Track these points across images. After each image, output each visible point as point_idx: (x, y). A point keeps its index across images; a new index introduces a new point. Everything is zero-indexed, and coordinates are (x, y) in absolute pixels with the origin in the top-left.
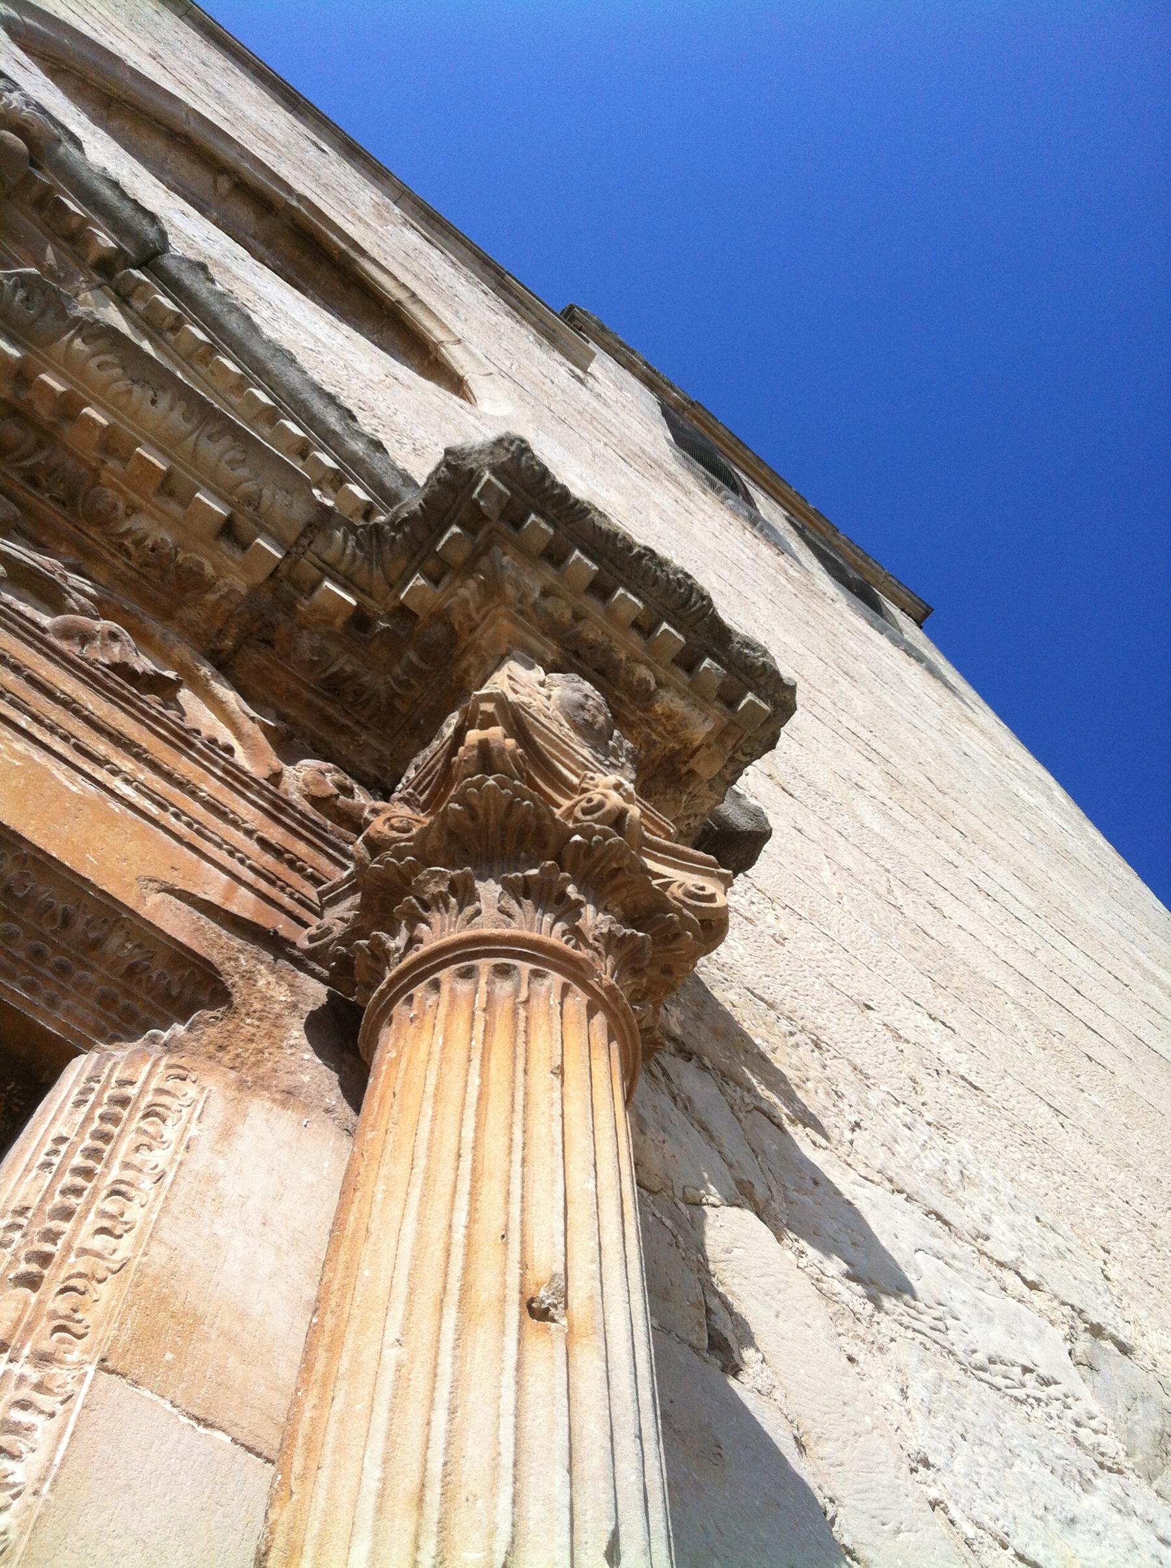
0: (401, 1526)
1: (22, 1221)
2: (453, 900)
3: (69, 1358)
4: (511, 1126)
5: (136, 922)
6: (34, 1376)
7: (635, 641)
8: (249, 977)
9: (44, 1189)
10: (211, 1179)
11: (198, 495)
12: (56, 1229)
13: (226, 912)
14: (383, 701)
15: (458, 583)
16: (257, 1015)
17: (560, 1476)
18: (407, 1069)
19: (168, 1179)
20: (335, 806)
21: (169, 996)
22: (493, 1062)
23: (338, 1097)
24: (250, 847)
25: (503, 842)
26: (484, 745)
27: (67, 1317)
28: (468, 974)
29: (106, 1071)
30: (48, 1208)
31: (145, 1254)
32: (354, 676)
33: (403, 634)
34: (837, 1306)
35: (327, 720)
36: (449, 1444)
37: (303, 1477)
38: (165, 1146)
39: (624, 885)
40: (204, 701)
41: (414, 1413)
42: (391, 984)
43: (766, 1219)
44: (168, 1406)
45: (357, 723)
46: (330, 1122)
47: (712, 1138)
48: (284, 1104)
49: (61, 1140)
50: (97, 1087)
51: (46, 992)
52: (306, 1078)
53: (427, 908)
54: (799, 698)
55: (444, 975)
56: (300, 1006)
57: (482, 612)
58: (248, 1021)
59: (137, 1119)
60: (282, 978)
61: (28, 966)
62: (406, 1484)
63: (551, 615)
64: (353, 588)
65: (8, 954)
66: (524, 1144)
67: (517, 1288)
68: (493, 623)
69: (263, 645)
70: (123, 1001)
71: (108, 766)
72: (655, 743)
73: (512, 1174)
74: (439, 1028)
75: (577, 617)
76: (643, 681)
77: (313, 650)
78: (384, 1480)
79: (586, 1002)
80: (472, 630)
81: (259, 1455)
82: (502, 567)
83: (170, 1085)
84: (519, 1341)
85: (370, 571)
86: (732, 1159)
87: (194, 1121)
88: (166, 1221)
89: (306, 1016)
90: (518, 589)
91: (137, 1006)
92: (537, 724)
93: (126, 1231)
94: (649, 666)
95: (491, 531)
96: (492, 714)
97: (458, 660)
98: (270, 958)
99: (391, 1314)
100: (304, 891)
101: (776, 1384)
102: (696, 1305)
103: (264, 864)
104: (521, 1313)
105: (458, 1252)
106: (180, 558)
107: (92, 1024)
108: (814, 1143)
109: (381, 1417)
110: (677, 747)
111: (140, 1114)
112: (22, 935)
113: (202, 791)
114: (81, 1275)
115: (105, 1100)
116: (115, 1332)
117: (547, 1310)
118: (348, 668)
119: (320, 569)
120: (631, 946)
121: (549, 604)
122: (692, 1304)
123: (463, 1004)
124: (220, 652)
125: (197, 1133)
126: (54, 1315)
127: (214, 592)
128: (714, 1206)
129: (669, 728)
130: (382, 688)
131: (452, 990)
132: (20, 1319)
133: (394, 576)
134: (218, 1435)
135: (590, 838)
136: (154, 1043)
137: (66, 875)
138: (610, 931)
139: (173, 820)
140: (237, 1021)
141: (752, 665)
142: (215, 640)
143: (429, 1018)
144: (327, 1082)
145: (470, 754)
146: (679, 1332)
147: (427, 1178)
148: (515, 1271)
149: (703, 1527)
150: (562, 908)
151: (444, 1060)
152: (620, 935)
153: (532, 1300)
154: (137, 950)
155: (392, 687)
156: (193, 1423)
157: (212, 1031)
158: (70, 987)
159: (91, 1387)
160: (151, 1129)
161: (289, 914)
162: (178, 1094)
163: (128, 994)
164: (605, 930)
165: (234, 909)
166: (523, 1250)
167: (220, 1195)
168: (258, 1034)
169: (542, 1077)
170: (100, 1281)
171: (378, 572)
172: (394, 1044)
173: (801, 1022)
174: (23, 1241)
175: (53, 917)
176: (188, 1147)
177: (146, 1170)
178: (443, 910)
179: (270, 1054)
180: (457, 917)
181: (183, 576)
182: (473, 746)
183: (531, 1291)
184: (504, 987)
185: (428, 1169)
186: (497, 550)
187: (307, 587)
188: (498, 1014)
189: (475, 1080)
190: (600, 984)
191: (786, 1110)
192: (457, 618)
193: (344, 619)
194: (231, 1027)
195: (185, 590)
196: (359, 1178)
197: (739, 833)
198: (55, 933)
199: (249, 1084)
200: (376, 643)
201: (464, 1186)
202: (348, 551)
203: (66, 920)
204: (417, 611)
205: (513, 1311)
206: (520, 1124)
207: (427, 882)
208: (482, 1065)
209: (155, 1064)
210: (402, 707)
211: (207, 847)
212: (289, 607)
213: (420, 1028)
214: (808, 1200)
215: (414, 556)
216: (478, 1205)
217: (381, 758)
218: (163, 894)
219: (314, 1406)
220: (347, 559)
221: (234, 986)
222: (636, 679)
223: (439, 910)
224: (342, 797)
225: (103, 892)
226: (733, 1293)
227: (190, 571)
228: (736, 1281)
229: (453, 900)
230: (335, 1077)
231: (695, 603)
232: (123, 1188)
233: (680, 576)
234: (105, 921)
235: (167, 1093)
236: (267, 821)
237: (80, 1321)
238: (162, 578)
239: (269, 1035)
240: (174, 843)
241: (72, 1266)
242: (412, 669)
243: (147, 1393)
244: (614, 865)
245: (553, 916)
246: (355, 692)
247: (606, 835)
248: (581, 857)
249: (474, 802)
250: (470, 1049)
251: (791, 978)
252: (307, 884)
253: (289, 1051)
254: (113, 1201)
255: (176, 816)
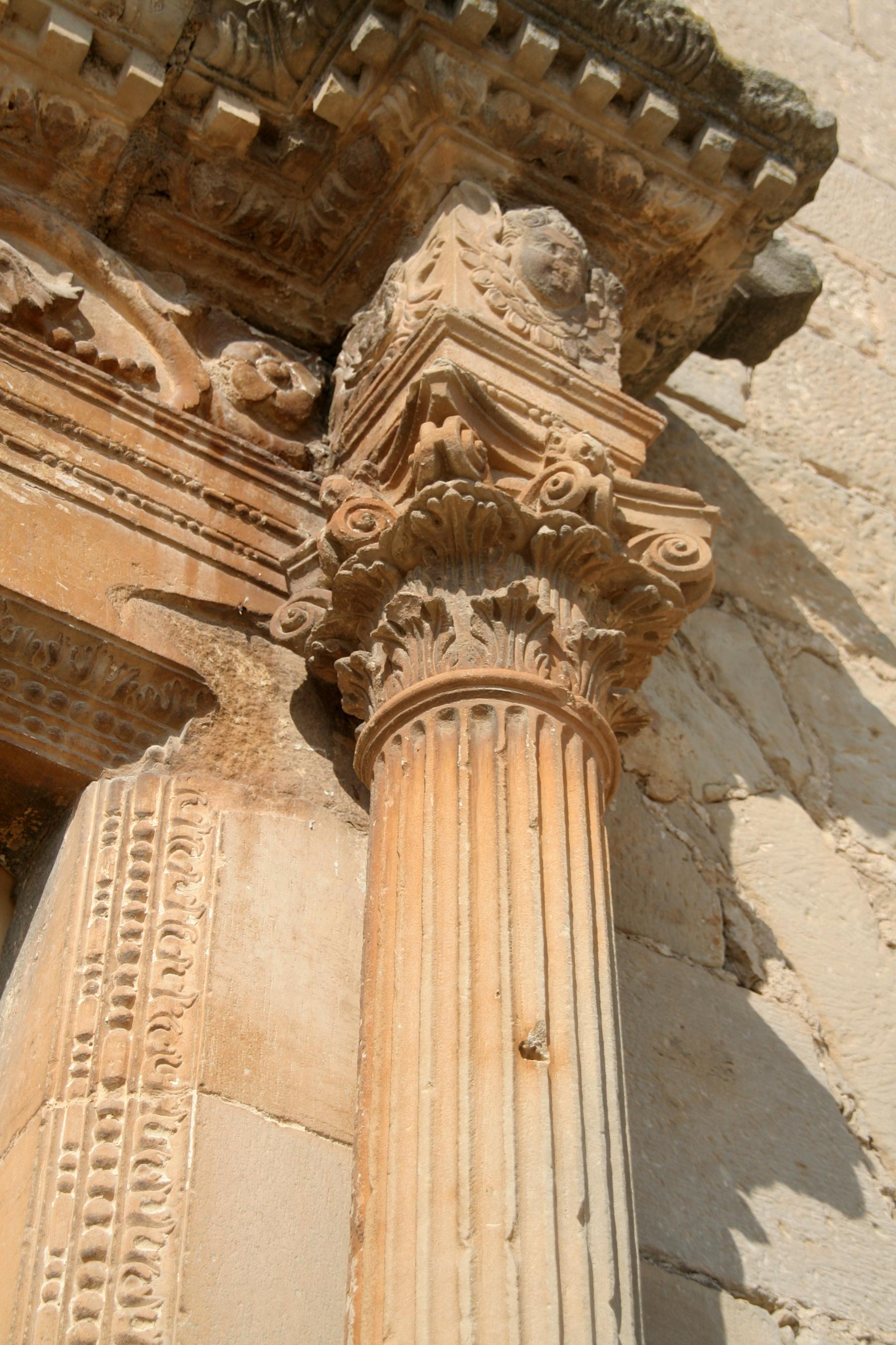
0: (447, 1210)
1: (100, 967)
2: (427, 625)
3: (175, 1084)
4: (498, 890)
5: (117, 645)
6: (154, 1102)
7: (615, 120)
8: (228, 668)
9: (107, 934)
10: (243, 907)
11: (52, 26)
12: (130, 973)
13: (193, 600)
14: (308, 238)
15: (383, 88)
16: (243, 711)
17: (547, 1172)
18: (406, 827)
19: (210, 913)
20: (274, 407)
21: (160, 710)
22: (480, 819)
23: (336, 787)
24: (199, 507)
25: (469, 542)
26: (440, 449)
27: (164, 1052)
28: (448, 716)
29: (123, 802)
30: (117, 952)
31: (209, 990)
32: (270, 212)
33: (321, 148)
34: (881, 888)
35: (244, 275)
36: (472, 1156)
37: (377, 1178)
38: (197, 878)
39: (598, 567)
40: (107, 300)
41: (447, 1133)
42: (379, 722)
43: (804, 798)
44: (255, 1111)
45: (281, 270)
46: (332, 817)
47: (742, 712)
48: (288, 809)
49: (105, 883)
50: (120, 820)
51: (49, 727)
52: (302, 772)
53: (401, 631)
54: (842, 138)
55: (426, 717)
56: (281, 686)
57: (418, 129)
58: (237, 720)
59: (165, 853)
60: (259, 658)
61: (29, 708)
62: (447, 1183)
63: (503, 122)
64: (251, 92)
65: (8, 700)
66: (510, 907)
67: (511, 1038)
68: (433, 143)
69: (156, 199)
70: (119, 722)
71: (45, 458)
72: (647, 256)
73: (502, 939)
74: (429, 785)
75: (536, 111)
76: (628, 180)
77: (217, 193)
78: (432, 1182)
79: (560, 731)
80: (408, 150)
81: (327, 1137)
82: (437, 72)
83: (185, 812)
84: (514, 1079)
85: (270, 67)
86: (764, 734)
87: (217, 851)
88: (218, 956)
89: (289, 697)
90: (459, 98)
91: (132, 725)
92: (497, 337)
93: (187, 968)
94: (632, 154)
95: (418, 23)
96: (444, 400)
97: (394, 189)
98: (241, 637)
99: (422, 1062)
100: (262, 546)
101: (798, 988)
102: (712, 922)
103: (217, 526)
104: (514, 1057)
105: (465, 1011)
106: (43, 105)
107: (96, 750)
108: (880, 676)
109: (425, 1139)
110: (677, 250)
111: (167, 847)
112: (17, 679)
113: (139, 455)
114: (163, 1014)
115: (131, 835)
116: (203, 1061)
117: (534, 1048)
118: (261, 205)
119: (208, 78)
120: (605, 646)
121: (499, 105)
122: (708, 921)
123: (447, 750)
124: (107, 219)
125: (223, 864)
126: (152, 1051)
127: (91, 145)
128: (740, 799)
129: (665, 231)
130: (304, 221)
131: (437, 737)
132: (127, 1057)
133: (301, 70)
134: (295, 1126)
135: (558, 529)
136: (156, 761)
137: (45, 613)
138: (583, 636)
139: (120, 501)
140: (227, 722)
141: (772, 119)
142: (101, 204)
143: (418, 764)
144: (322, 771)
145: (427, 459)
146: (692, 955)
147: (435, 943)
148: (508, 1022)
149: (710, 1139)
150: (532, 624)
151: (438, 820)
152: (592, 638)
153: (523, 1043)
154: (123, 672)
155: (316, 221)
156: (275, 1121)
157: (206, 739)
158: (69, 719)
159: (198, 1107)
160: (181, 863)
161: (253, 580)
162: (196, 821)
163: (122, 714)
164: (577, 637)
165: (200, 594)
166: (514, 1006)
167: (254, 920)
168: (249, 732)
169: (524, 834)
170: (179, 1016)
171: (280, 68)
172: (390, 791)
173: (885, 490)
174: (107, 986)
175: (41, 656)
176: (218, 881)
177: (187, 906)
178: (418, 635)
179: (264, 751)
180: (432, 644)
181: (52, 133)
182: (429, 450)
183: (521, 1038)
184: (484, 727)
185: (435, 934)
186: (427, 49)
187: (196, 102)
188: (480, 762)
189: (466, 846)
190: (573, 708)
191: (845, 641)
192: (387, 137)
193: (248, 142)
194: (222, 731)
195: (56, 150)
196: (380, 934)
197: (776, 299)
198: (45, 670)
199: (254, 795)
200: (288, 165)
201: (465, 953)
202: (240, 47)
203: (54, 657)
204: (335, 122)
205: (509, 1055)
206: (505, 889)
207: (399, 607)
208: (470, 828)
209: (166, 791)
210: (332, 244)
211: (159, 525)
212: (180, 141)
213: (412, 778)
214: (861, 760)
215: (323, 42)
216: (478, 965)
217: (314, 308)
218: (134, 600)
219: (377, 1128)
220: (240, 58)
221: (217, 686)
222: (618, 178)
223: (414, 635)
224: (280, 392)
225: (81, 622)
226: (756, 897)
227: (60, 126)
228: (761, 883)
229: (427, 625)
230: (330, 765)
231: (691, 51)
232: (174, 927)
233: (669, 15)
234: (89, 649)
235: (185, 822)
236: (212, 468)
237: (173, 1053)
238: (26, 138)
239: (259, 731)
240: (127, 530)
241: (154, 1006)
242: (338, 197)
243: (238, 1105)
244: (585, 552)
245: (525, 635)
246: (272, 232)
247: (575, 524)
248: (551, 547)
249: (437, 510)
250: (458, 811)
251: (878, 417)
252: (264, 535)
253: (281, 745)
254: (169, 941)
255: (122, 496)
